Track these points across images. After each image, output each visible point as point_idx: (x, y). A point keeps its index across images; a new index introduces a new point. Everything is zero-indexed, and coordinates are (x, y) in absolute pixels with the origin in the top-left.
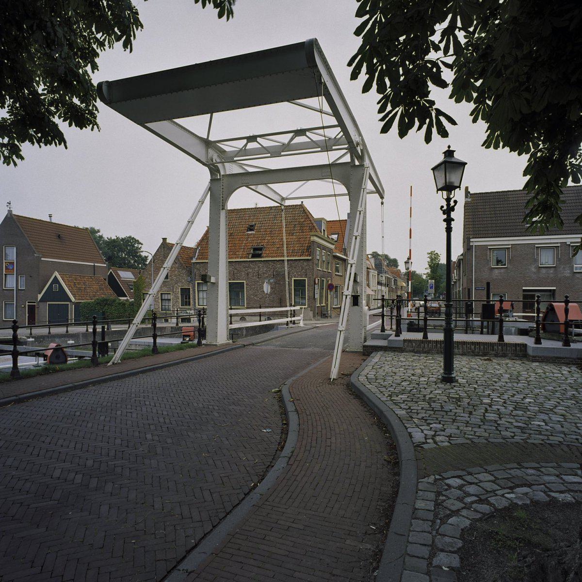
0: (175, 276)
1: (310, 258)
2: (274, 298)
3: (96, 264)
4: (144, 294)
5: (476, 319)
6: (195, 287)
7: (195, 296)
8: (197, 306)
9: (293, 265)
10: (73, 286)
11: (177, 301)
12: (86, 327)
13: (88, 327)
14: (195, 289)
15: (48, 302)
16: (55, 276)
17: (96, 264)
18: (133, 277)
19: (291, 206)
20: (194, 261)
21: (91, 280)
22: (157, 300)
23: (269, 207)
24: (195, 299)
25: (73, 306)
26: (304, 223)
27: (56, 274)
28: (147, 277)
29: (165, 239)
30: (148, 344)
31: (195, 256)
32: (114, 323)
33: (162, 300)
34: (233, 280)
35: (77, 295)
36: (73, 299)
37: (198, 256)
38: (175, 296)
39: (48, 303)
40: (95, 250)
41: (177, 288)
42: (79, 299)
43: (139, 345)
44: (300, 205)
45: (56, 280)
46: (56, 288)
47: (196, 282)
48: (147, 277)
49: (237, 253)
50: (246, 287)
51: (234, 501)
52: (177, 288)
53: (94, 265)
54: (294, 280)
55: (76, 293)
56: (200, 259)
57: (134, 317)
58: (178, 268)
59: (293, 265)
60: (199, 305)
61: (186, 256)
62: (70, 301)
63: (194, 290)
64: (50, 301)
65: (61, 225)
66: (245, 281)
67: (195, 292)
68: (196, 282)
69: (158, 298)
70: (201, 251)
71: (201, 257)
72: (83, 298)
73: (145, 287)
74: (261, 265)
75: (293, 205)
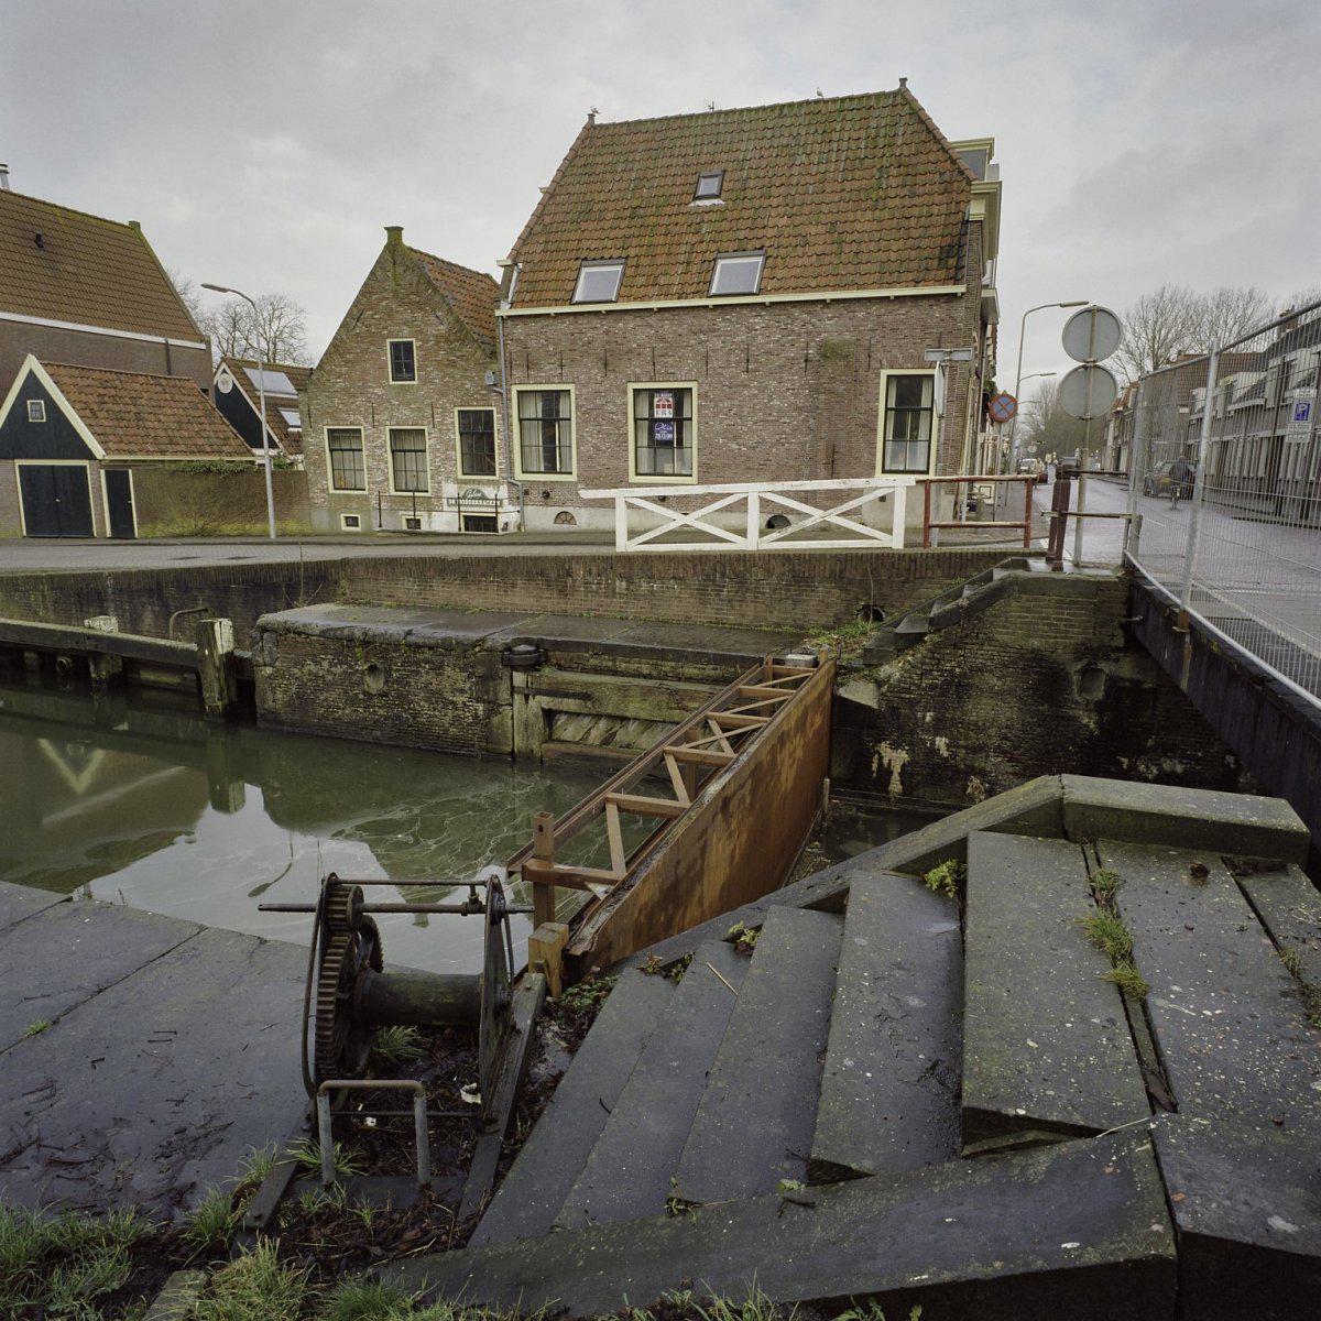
1: (960, 289)
2: (803, 444)
3: (171, 341)
7: (509, 437)
8: (519, 476)
9: (888, 318)
10: (95, 407)
11: (448, 458)
12: (540, 416)
13: (540, 422)
15: (20, 457)
16: (31, 372)
17: (171, 341)
18: (292, 389)
19: (860, 98)
20: (504, 310)
21: (158, 388)
22: (378, 452)
23: (772, 108)
24: (511, 452)
25: (102, 472)
26: (914, 160)
27: (32, 363)
29: (395, 232)
31: (507, 297)
34: (651, 380)
35: (111, 437)
36: (98, 451)
37: (517, 292)
39: (19, 462)
40: (172, 306)
42: (118, 451)
44: (895, 94)
45: (33, 387)
46: (36, 412)
49: (662, 280)
50: (700, 406)
51: (663, 1092)
53: (167, 344)
55: (108, 430)
56: (523, 303)
57: (610, 861)
59: (888, 318)
61: (472, 301)
62: (90, 456)
64: (26, 457)
65: (44, 203)
69: (384, 446)
70: (526, 277)
71: (528, 296)
72: (135, 448)
74: (757, 322)
75: (868, 96)
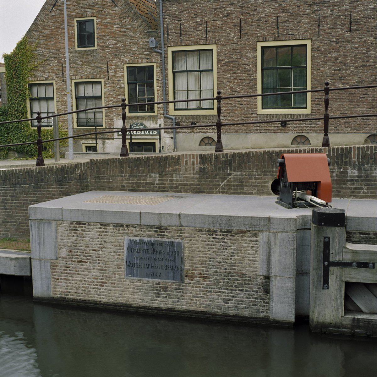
0: (114, 36)
4: (31, 86)
5: (106, 121)
6: (166, 63)
14: (166, 69)
28: (39, 43)
30: (155, 222)
32: (29, 172)
33: (78, 99)
34: (276, 40)
38: (113, 88)
41: (117, 66)
43: (117, 226)
47: (170, 50)
48: (39, 43)
50: (313, 58)
52: (117, 66)
54: (306, 45)
58: (120, 18)
60: (175, 109)
63: (164, 71)
66: (308, 43)
67: (166, 76)
68: (170, 50)
73: (35, 68)
